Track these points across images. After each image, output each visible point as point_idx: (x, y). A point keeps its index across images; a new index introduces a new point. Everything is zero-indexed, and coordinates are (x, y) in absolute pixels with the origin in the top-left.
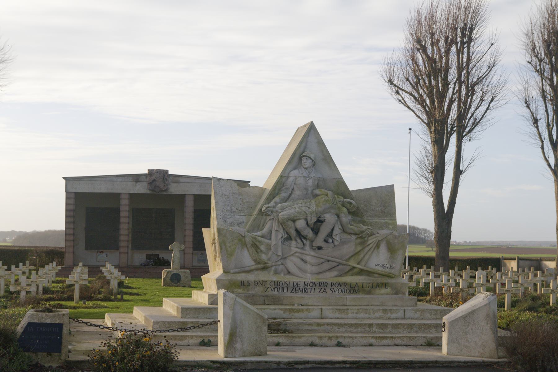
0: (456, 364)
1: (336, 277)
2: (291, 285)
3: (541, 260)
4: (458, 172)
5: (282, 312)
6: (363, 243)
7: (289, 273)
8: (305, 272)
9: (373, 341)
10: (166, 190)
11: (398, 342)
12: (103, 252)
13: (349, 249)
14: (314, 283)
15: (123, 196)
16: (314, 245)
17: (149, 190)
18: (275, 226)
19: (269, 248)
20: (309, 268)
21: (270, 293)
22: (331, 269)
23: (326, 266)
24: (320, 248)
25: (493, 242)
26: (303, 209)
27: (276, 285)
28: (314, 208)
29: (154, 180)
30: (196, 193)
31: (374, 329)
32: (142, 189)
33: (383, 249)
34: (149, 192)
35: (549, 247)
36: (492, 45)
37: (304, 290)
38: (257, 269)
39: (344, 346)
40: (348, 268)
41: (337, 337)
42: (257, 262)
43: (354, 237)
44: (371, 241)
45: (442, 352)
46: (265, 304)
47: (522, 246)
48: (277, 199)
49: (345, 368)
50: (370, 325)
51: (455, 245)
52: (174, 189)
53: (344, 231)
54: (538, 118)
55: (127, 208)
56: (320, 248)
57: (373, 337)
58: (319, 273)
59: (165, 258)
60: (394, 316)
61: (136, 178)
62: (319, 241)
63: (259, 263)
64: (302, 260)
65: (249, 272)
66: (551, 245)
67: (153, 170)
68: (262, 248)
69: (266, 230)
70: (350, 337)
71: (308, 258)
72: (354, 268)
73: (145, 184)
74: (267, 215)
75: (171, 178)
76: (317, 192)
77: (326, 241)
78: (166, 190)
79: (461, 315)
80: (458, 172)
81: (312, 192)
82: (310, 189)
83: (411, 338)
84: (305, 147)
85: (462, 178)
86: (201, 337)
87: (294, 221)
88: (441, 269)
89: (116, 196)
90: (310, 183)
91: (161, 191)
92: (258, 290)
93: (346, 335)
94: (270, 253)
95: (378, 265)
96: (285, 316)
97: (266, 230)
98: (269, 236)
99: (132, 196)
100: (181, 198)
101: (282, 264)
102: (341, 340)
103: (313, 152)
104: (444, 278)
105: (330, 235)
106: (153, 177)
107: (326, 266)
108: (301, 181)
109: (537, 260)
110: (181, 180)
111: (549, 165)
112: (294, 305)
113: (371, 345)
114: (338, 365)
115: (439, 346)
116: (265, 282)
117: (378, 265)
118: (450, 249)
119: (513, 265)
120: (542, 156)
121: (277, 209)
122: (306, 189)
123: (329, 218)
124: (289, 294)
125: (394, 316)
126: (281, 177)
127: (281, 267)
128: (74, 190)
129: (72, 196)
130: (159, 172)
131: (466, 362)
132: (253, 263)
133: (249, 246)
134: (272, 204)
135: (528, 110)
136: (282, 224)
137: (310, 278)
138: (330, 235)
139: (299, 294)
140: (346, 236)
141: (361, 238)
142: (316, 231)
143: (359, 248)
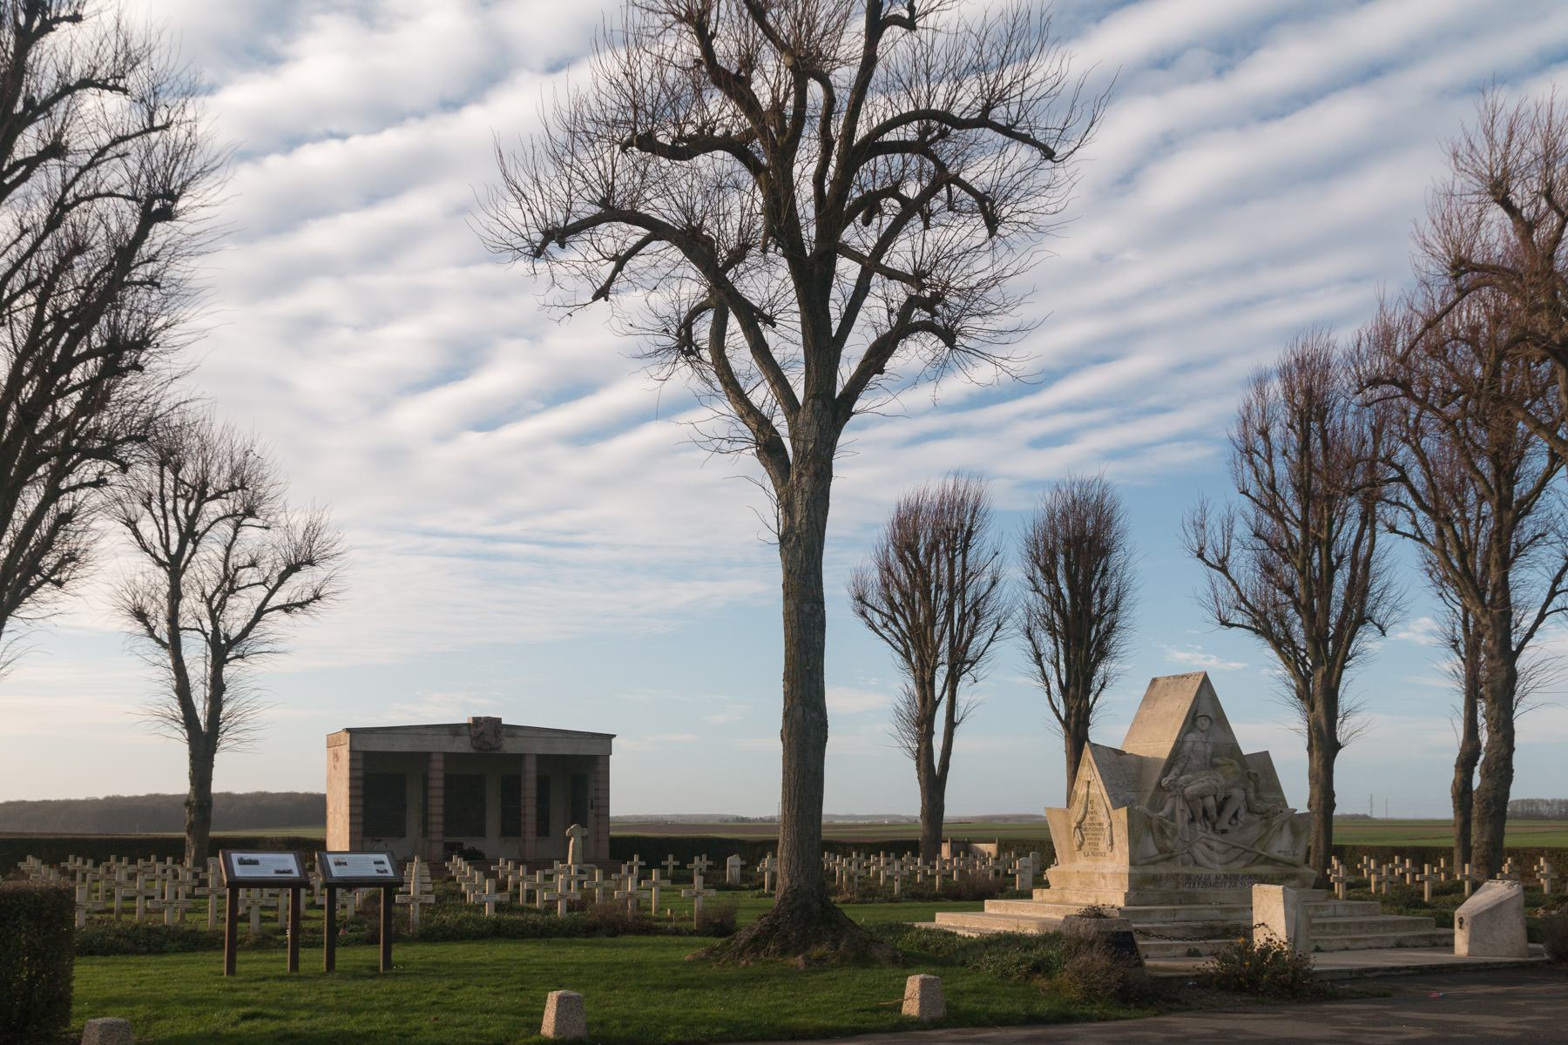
0: (1377, 974)
1: (1244, 867)
2: (1203, 879)
3: (970, 842)
4: (951, 725)
5: (1218, 912)
6: (1268, 825)
7: (1196, 863)
8: (1212, 861)
9: (1348, 944)
10: (498, 748)
11: (1372, 944)
12: (379, 841)
13: (1254, 832)
14: (1225, 876)
15: (434, 757)
16: (1217, 827)
17: (475, 748)
18: (1180, 805)
19: (1175, 832)
20: (1217, 857)
21: (1182, 889)
22: (1237, 858)
23: (1233, 854)
24: (1224, 832)
25: (637, 817)
26: (1214, 782)
27: (1188, 878)
28: (1223, 781)
29: (482, 733)
30: (541, 752)
31: (1328, 930)
32: (462, 746)
33: (1286, 832)
34: (472, 751)
35: (718, 823)
36: (997, 554)
37: (1215, 885)
38: (1162, 860)
39: (1322, 951)
40: (1254, 856)
41: (1316, 940)
42: (1161, 850)
43: (1257, 817)
44: (1276, 821)
45: (1452, 951)
46: (1181, 903)
47: (702, 822)
48: (1175, 770)
49: (1408, 975)
50: (1324, 925)
51: (887, 825)
52: (509, 747)
53: (1249, 811)
54: (1042, 651)
55: (441, 775)
56: (1224, 832)
57: (1348, 939)
58: (1227, 863)
59: (477, 848)
60: (1324, 913)
61: (454, 730)
62: (1223, 824)
63: (1165, 852)
64: (1208, 847)
65: (1154, 863)
66: (721, 820)
67: (480, 718)
68: (1168, 832)
69: (1167, 810)
70: (1327, 940)
71: (1215, 844)
72: (1260, 855)
73: (467, 739)
74: (1170, 791)
75: (505, 730)
76: (1217, 760)
77: (1230, 823)
78: (498, 748)
79: (1486, 908)
80: (951, 725)
81: (1211, 762)
82: (1209, 757)
83: (1382, 939)
84: (1198, 706)
85: (957, 730)
86: (1187, 945)
87: (1203, 797)
88: (892, 855)
89: (425, 757)
90: (1209, 749)
91: (492, 749)
92: (1168, 886)
93: (1322, 937)
94: (1176, 839)
95: (1279, 852)
96: (1223, 917)
97: (1167, 810)
98: (1172, 817)
99: (449, 757)
100: (519, 758)
101: (1188, 853)
102: (1319, 944)
103: (1206, 708)
104: (897, 865)
105: (1235, 815)
106: (480, 729)
107: (1233, 854)
108: (1200, 747)
109: (964, 842)
110: (519, 733)
111: (1059, 717)
112: (1210, 904)
113: (1347, 949)
114: (1402, 972)
115: (1450, 946)
116: (1178, 875)
117: (1279, 852)
118: (1507, 830)
119: (990, 848)
120: (1048, 702)
121: (1180, 783)
122: (1205, 757)
123: (1237, 793)
124: (1200, 890)
125: (1324, 913)
126: (1177, 741)
127: (1187, 856)
128: (363, 749)
129: (360, 756)
130: (489, 720)
131: (1511, 963)
132: (1157, 852)
133: (1155, 830)
134: (1171, 776)
135: (1029, 643)
136: (1186, 801)
137: (1220, 870)
138: (1235, 815)
139: (1210, 890)
140: (1250, 817)
141: (1266, 818)
142: (1220, 809)
143: (1264, 831)
